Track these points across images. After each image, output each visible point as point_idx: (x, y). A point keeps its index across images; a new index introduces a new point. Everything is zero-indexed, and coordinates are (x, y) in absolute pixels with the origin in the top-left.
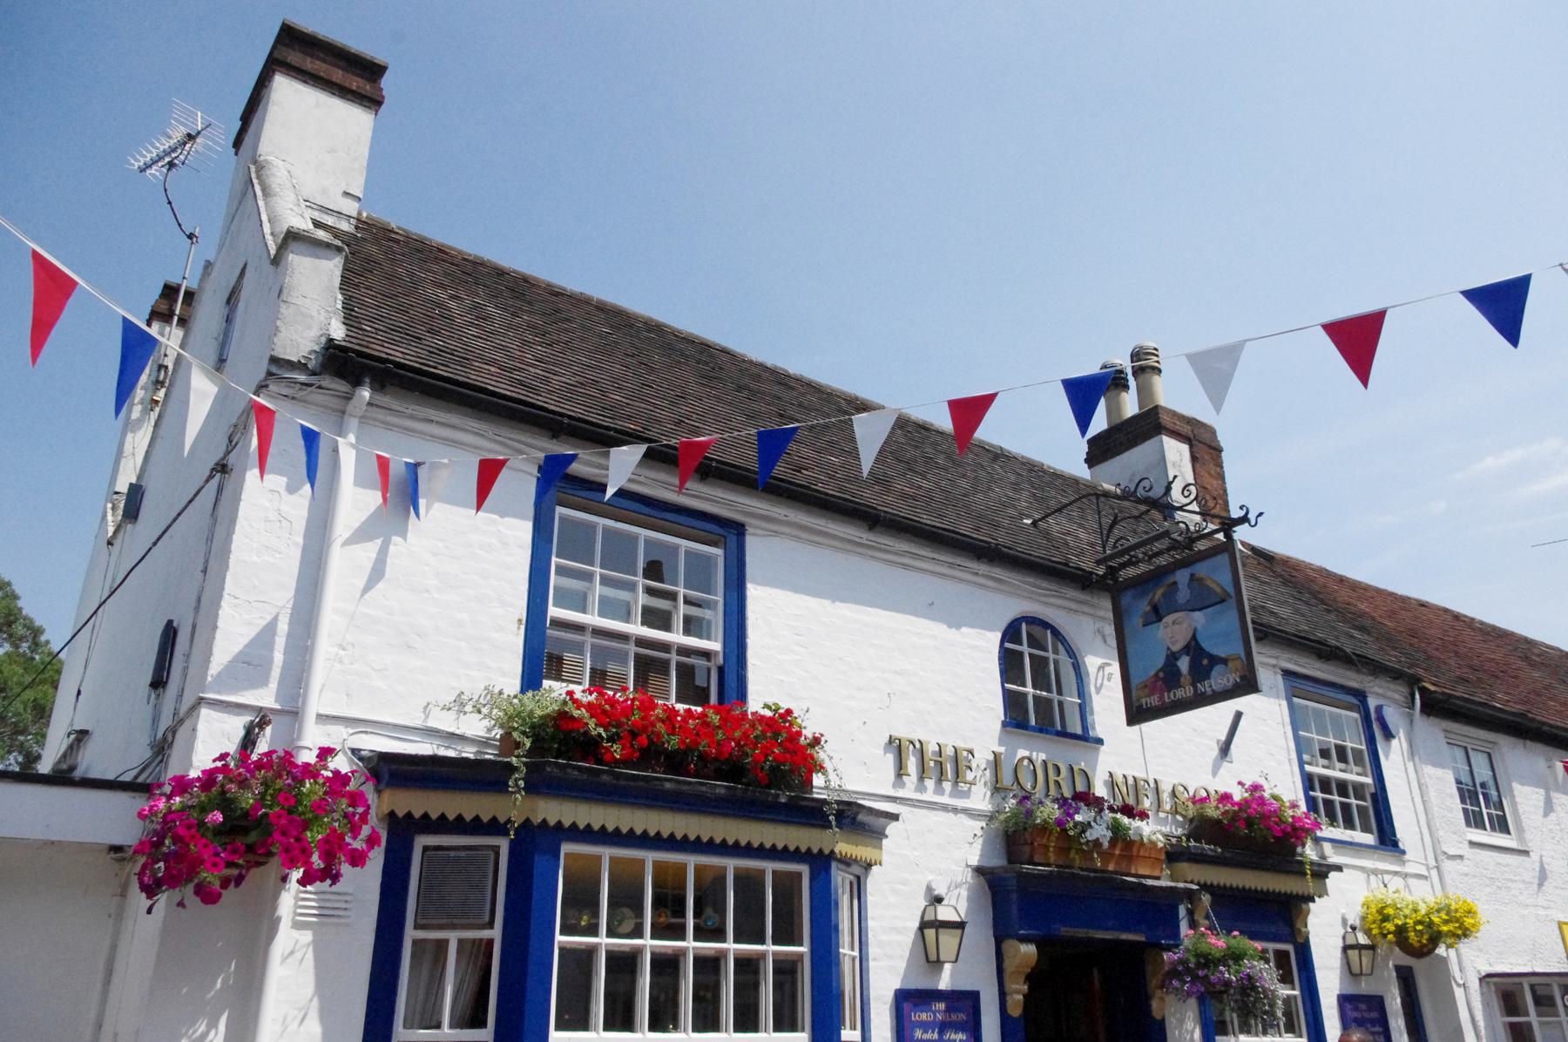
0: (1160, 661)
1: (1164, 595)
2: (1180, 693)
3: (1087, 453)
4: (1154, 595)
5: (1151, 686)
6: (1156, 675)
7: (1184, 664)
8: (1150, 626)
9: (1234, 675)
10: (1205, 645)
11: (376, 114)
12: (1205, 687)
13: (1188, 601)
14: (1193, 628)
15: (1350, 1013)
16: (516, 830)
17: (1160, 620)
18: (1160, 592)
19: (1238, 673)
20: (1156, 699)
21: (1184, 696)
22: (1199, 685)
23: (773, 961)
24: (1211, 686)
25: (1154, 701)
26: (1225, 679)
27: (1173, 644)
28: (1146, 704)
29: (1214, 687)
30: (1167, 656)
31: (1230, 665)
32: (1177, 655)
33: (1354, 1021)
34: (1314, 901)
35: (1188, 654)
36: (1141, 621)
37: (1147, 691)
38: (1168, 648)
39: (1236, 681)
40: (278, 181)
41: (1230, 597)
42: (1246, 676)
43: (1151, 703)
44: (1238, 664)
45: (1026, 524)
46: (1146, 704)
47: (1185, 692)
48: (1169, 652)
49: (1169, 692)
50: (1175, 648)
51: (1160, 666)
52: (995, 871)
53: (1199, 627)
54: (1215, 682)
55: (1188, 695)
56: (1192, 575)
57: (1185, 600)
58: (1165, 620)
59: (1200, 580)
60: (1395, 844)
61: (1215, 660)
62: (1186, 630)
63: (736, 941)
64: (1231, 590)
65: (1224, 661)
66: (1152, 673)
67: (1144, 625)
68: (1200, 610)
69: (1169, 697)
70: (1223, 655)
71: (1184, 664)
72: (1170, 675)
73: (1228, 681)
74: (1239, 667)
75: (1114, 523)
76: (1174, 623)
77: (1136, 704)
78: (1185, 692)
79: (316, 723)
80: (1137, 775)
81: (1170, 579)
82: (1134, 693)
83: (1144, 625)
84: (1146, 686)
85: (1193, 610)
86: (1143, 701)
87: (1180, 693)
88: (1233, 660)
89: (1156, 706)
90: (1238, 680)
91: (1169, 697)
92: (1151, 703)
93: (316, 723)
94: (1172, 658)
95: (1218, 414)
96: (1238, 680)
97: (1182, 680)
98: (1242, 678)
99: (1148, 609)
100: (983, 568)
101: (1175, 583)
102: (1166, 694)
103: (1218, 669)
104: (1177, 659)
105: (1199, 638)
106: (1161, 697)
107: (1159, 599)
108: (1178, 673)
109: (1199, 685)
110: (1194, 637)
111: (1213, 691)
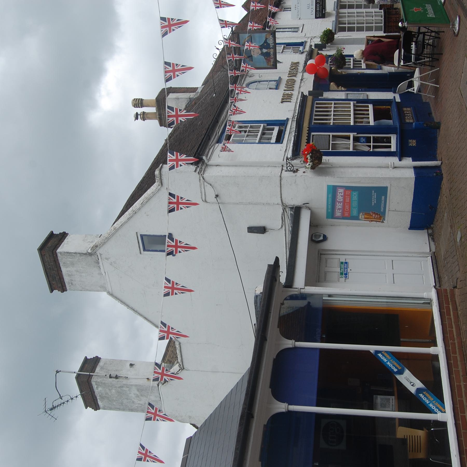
2: (272, 53)
3: (92, 409)
5: (268, 61)
6: (266, 59)
7: (265, 51)
12: (271, 45)
16: (379, 64)
23: (318, 405)
25: (272, 60)
27: (259, 53)
28: (272, 63)
30: (261, 55)
31: (267, 37)
32: (262, 52)
34: (309, 92)
36: (251, 62)
37: (269, 62)
38: (260, 55)
41: (251, 35)
44: (268, 35)
45: (215, 96)
46: (272, 63)
49: (271, 56)
50: (260, 53)
51: (264, 57)
52: (244, 407)
58: (252, 55)
60: (303, 42)
61: (266, 42)
63: (371, 143)
65: (266, 39)
67: (252, 61)
69: (272, 56)
71: (265, 51)
72: (266, 55)
73: (271, 39)
76: (253, 52)
77: (272, 66)
78: (272, 51)
79: (328, 186)
80: (288, 74)
82: (269, 66)
84: (268, 63)
86: (272, 64)
87: (272, 53)
89: (342, 205)
91: (272, 56)
93: (328, 186)
94: (262, 54)
97: (269, 52)
98: (271, 34)
99: (248, 59)
104: (263, 52)
106: (272, 58)
108: (266, 53)
111: (273, 43)
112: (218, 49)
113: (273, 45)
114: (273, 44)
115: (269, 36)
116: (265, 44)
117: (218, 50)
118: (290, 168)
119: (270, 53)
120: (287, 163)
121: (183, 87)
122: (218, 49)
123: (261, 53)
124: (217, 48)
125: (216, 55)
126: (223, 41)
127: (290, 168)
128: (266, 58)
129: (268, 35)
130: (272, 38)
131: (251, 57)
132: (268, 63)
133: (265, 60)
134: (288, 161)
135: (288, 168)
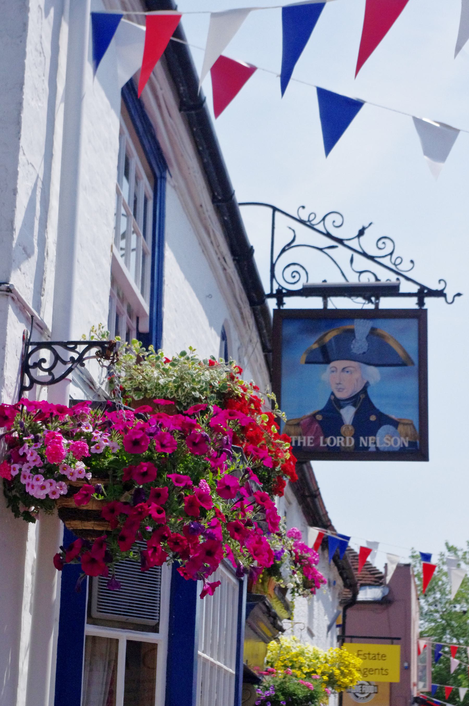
0: (321, 404)
1: (337, 338)
2: (338, 441)
4: (325, 335)
6: (314, 416)
8: (313, 365)
9: (402, 439)
10: (375, 401)
11: (20, 270)
13: (364, 353)
14: (365, 382)
15: (346, 679)
17: (328, 362)
18: (331, 335)
19: (407, 438)
20: (309, 441)
21: (343, 445)
22: (362, 438)
24: (375, 443)
26: (393, 440)
27: (339, 390)
28: (296, 442)
29: (378, 445)
30: (330, 400)
31: (400, 427)
32: (342, 403)
33: (322, 676)
35: (354, 405)
36: (303, 358)
37: (299, 430)
38: (333, 394)
39: (403, 444)
40: (279, 605)
41: (413, 363)
42: (416, 443)
43: (302, 443)
44: (409, 430)
47: (345, 443)
48: (333, 397)
49: (326, 437)
50: (339, 395)
53: (372, 382)
54: (381, 440)
55: (348, 445)
56: (373, 330)
57: (361, 352)
59: (381, 337)
62: (357, 380)
64: (415, 358)
65: (395, 423)
66: (309, 413)
67: (307, 362)
68: (376, 365)
70: (393, 417)
73: (396, 442)
74: (409, 433)
75: (289, 246)
76: (344, 369)
81: (348, 326)
83: (307, 362)
84: (298, 424)
85: (369, 364)
87: (338, 441)
88: (404, 424)
89: (307, 447)
90: (407, 445)
91: (325, 443)
92: (302, 443)
95: (418, 122)
96: (407, 445)
97: (343, 429)
100: (145, 290)
101: (352, 332)
102: (322, 438)
103: (384, 430)
104: (341, 407)
105: (369, 391)
106: (316, 440)
107: (330, 341)
108: (340, 422)
109: (362, 438)
110: (364, 390)
111: (377, 448)
112: (361, 233)
113: (368, 448)
114: (372, 448)
115: (406, 435)
116: (373, 418)
117: (356, 233)
118: (46, 366)
119: (338, 433)
120: (81, 348)
121: (23, 133)
122: (361, 233)
123: (337, 401)
124: (366, 231)
125: (337, 224)
126: (391, 254)
127: (46, 366)
128: (319, 417)
129: (409, 430)
130: (399, 444)
131: (321, 358)
132: (298, 424)
133: (309, 413)
134: (94, 351)
135: (45, 353)
